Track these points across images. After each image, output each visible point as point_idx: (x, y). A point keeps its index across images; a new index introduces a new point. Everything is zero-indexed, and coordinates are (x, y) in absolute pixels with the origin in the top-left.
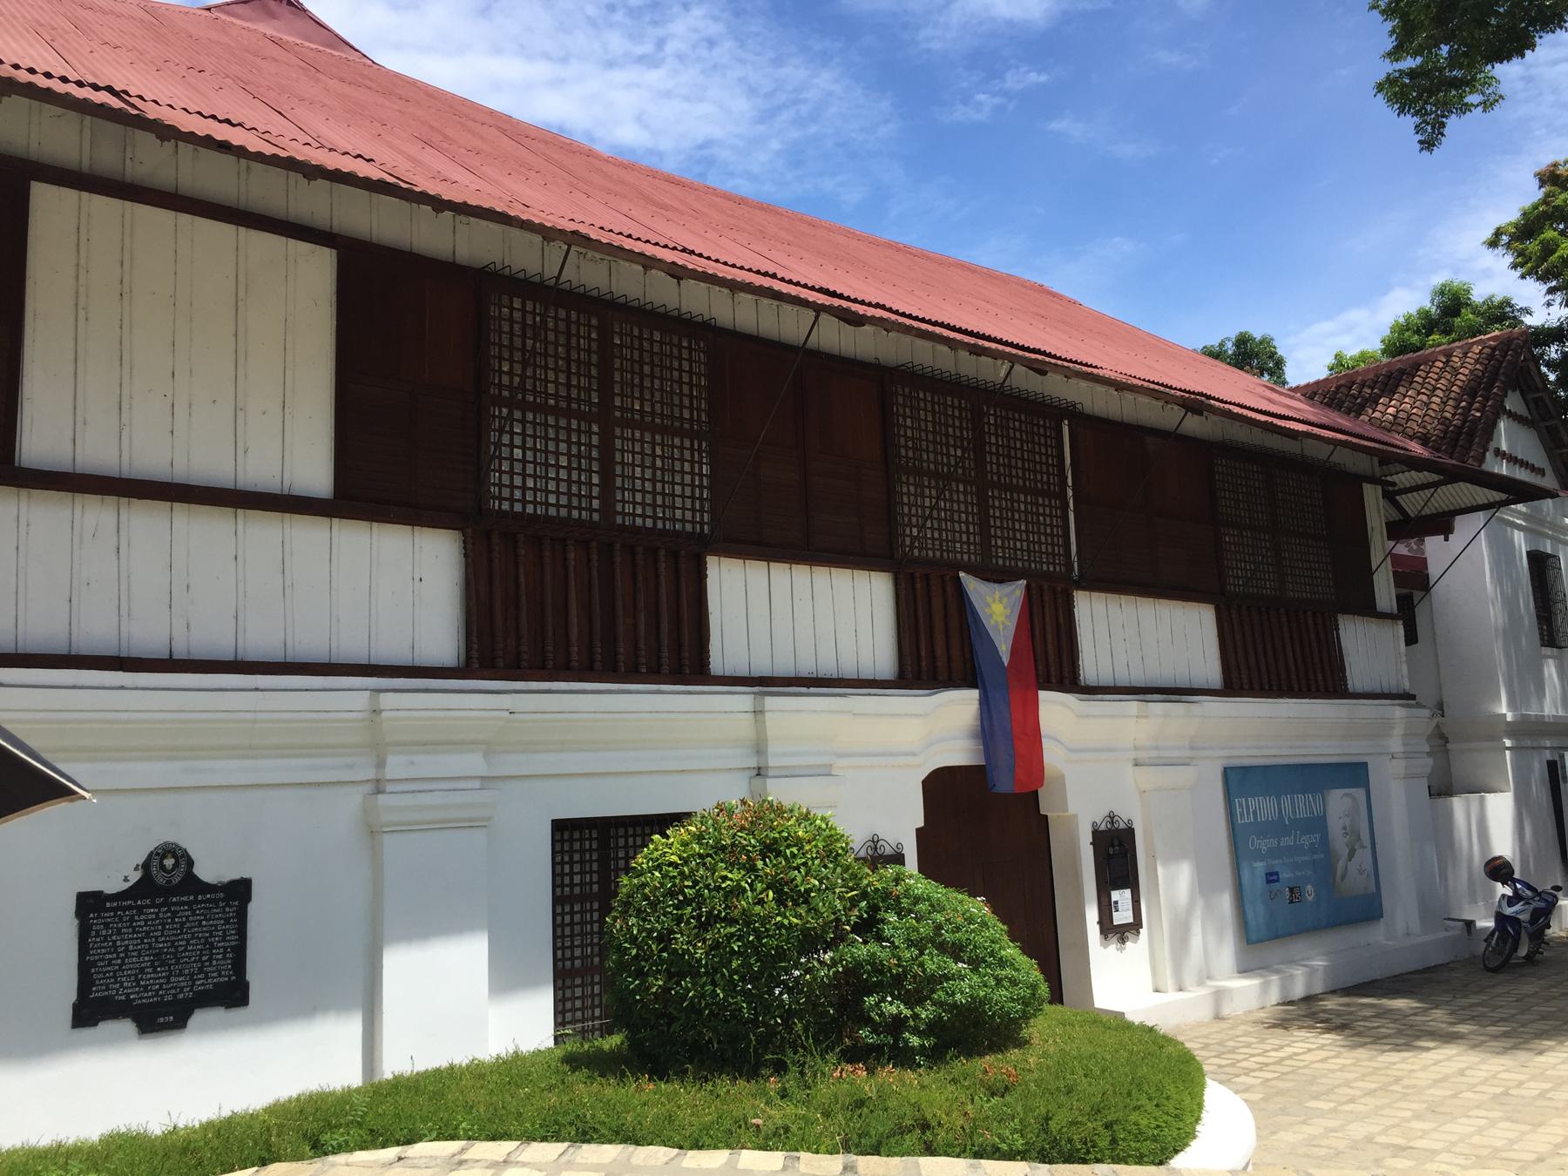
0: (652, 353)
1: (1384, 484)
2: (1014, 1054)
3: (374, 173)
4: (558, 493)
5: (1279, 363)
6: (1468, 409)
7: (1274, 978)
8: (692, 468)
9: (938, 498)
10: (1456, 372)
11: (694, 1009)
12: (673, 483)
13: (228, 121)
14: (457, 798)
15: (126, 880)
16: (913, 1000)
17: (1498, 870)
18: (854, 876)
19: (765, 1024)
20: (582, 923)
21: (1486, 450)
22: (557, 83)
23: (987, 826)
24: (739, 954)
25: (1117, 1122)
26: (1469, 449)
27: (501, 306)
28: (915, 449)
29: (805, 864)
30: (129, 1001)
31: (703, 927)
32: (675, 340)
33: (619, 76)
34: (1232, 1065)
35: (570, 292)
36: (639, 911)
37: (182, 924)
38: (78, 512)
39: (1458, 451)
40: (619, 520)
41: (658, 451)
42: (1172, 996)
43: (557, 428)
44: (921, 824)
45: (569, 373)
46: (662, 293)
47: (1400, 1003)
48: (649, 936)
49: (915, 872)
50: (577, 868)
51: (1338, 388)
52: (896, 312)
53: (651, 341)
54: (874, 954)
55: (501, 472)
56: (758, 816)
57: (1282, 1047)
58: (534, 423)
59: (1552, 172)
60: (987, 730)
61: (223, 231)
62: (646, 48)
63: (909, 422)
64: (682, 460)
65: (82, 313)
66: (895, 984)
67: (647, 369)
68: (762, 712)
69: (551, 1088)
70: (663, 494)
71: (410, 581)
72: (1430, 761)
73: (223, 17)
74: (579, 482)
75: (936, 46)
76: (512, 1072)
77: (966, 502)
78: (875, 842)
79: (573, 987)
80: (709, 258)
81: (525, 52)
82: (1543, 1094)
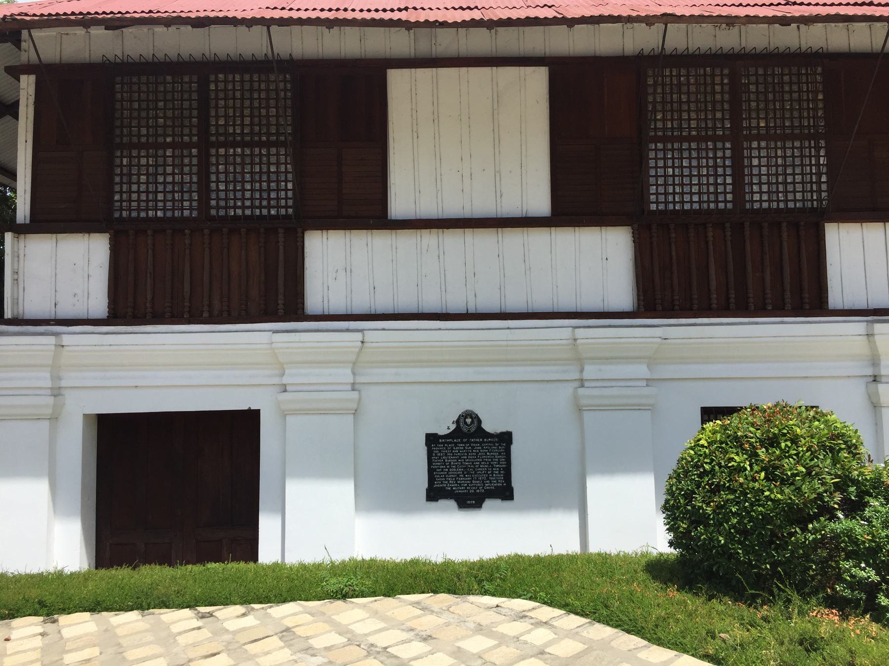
14: (628, 392)
24: (734, 514)
40: (748, 206)
67: (771, 96)
71: (601, 260)
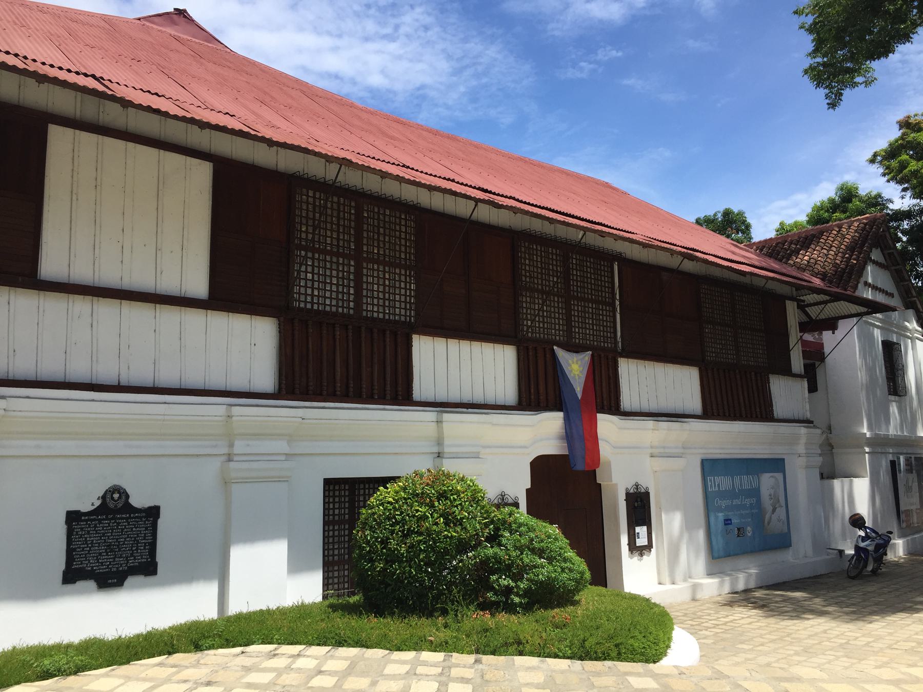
0: (385, 222)
1: (799, 301)
2: (570, 609)
3: (238, 126)
4: (331, 298)
5: (748, 227)
6: (849, 259)
7: (727, 578)
8: (406, 285)
9: (543, 305)
10: (844, 237)
11: (399, 580)
12: (395, 294)
13: (157, 94)
15: (93, 505)
16: (517, 577)
17: (857, 521)
18: (487, 512)
19: (437, 589)
20: (339, 536)
21: (858, 282)
22: (335, 49)
23: (567, 488)
24: (424, 551)
25: (621, 644)
26: (849, 281)
27: (302, 195)
28: (530, 277)
29: (461, 504)
30: (93, 570)
31: (405, 536)
32: (398, 215)
33: (371, 46)
34: (698, 625)
35: (340, 188)
36: (371, 527)
37: (122, 529)
38: (71, 304)
39: (843, 280)
40: (364, 314)
41: (387, 276)
42: (669, 587)
43: (331, 262)
44: (529, 486)
45: (338, 232)
46: (391, 189)
47: (798, 594)
48: (376, 540)
49: (525, 512)
50: (337, 506)
51: (777, 244)
52: (521, 202)
53: (384, 214)
54: (496, 553)
55: (300, 286)
56: (436, 478)
57: (727, 616)
58: (319, 259)
59: (907, 121)
60: (569, 436)
61: (152, 152)
62: (388, 30)
63: (527, 262)
64: (400, 281)
65: (74, 197)
66: (507, 569)
67: (382, 230)
68: (441, 422)
69: (322, 620)
70: (389, 300)
71: (248, 345)
72: (821, 459)
73: (147, 24)
74: (343, 293)
75: (557, 33)
76: (301, 612)
77: (558, 307)
78: (503, 495)
79: (333, 571)
80: (417, 170)
81: (317, 31)
82: (867, 644)
